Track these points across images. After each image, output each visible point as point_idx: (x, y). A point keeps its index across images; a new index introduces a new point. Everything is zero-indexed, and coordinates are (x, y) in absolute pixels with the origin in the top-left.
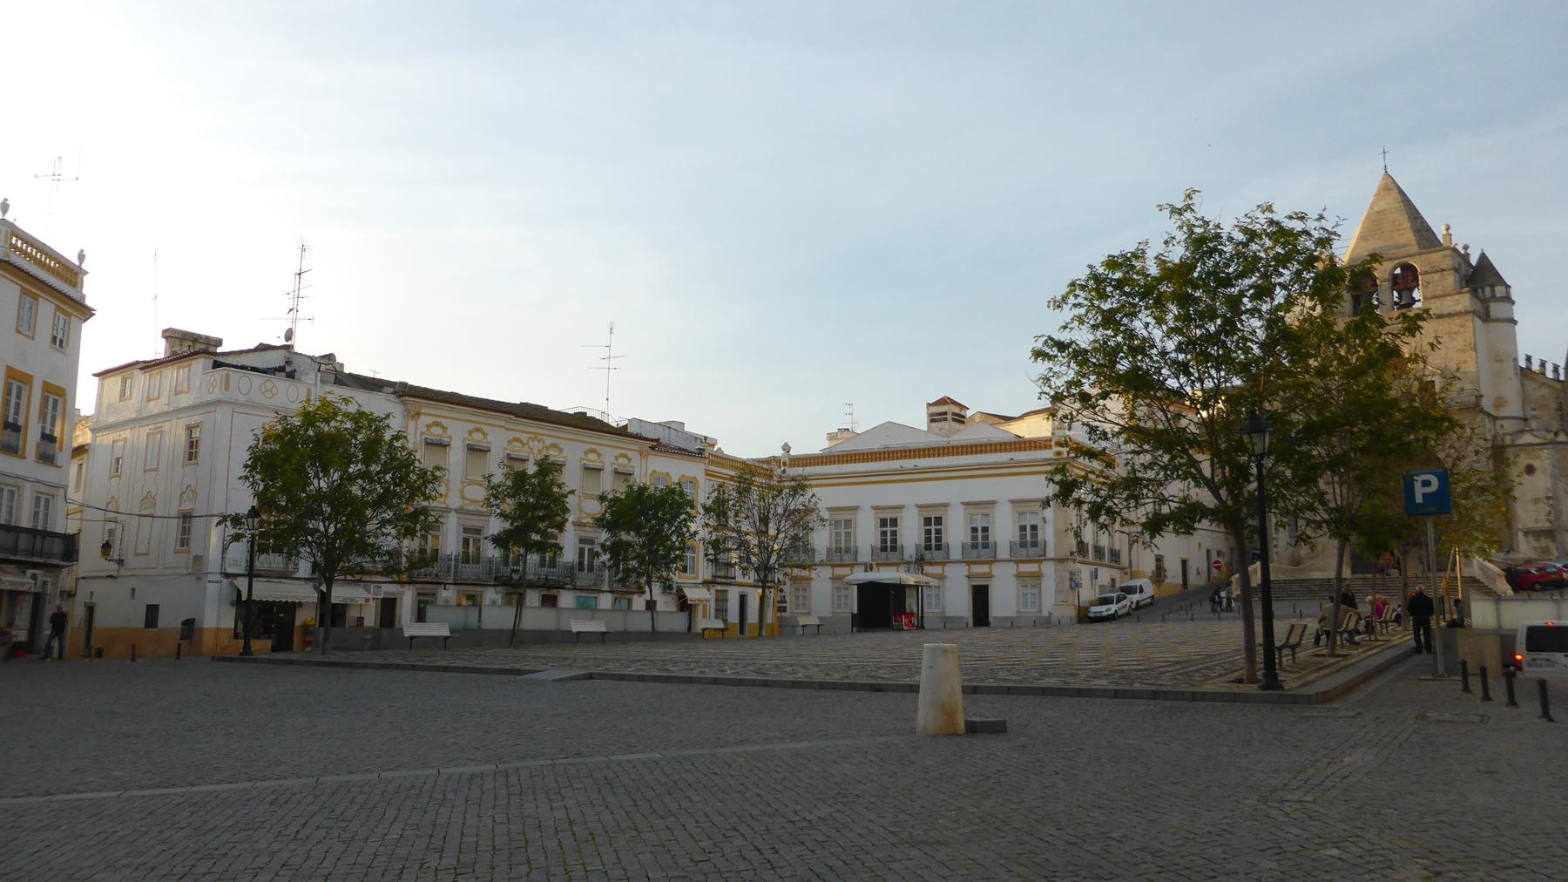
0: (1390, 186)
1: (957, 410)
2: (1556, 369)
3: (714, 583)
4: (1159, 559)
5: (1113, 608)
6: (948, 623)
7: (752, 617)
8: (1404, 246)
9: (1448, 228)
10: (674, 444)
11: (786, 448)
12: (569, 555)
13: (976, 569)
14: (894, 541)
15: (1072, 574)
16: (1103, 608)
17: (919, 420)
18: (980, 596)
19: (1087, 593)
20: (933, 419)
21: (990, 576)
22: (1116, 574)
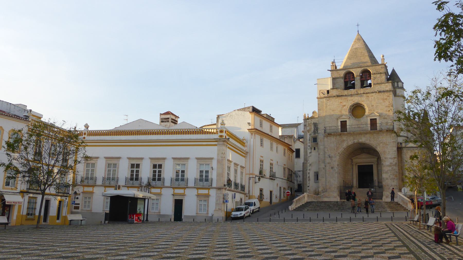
0: (360, 39)
1: (174, 118)
3: (27, 192)
4: (261, 190)
5: (243, 213)
6: (161, 221)
7: (53, 211)
8: (365, 63)
9: (383, 56)
10: (12, 113)
11: (87, 126)
14: (137, 175)
15: (224, 195)
16: (238, 213)
17: (156, 120)
18: (178, 204)
19: (231, 205)
20: (162, 121)
21: (184, 195)
22: (243, 196)
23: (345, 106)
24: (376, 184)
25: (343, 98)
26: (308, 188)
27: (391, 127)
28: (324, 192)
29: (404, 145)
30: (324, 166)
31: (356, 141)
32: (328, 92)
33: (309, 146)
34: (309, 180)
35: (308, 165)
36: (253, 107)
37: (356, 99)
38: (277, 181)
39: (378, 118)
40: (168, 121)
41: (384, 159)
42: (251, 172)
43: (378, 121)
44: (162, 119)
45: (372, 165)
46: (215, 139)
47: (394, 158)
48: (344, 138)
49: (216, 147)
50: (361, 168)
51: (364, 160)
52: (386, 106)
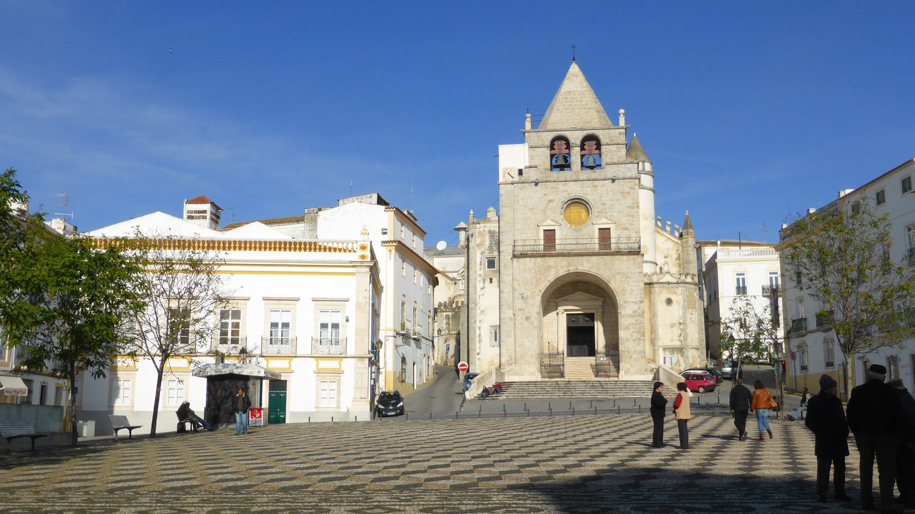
12: (97, 367)
23: (551, 201)
26: (478, 357)
27: (636, 246)
28: (511, 364)
29: (655, 279)
31: (572, 269)
32: (520, 172)
33: (480, 275)
34: (480, 341)
35: (478, 312)
37: (575, 190)
40: (205, 218)
41: (622, 303)
43: (613, 234)
48: (551, 261)
49: (353, 278)
52: (628, 207)
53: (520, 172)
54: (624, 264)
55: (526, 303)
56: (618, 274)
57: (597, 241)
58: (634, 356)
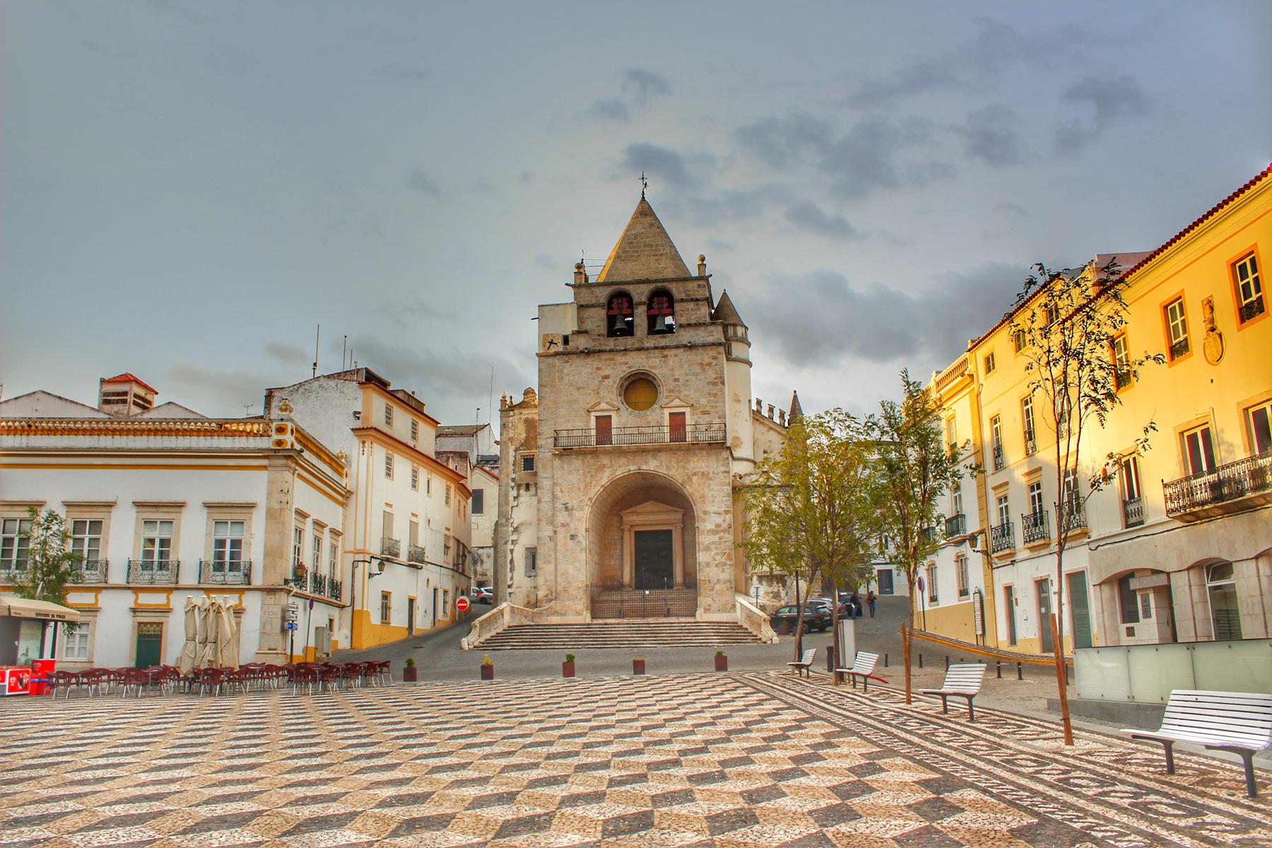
1: (142, 392)
2: (782, 415)
4: (386, 596)
13: (147, 599)
17: (91, 397)
23: (607, 377)
24: (678, 578)
25: (604, 356)
26: (510, 590)
27: (720, 435)
30: (551, 534)
32: (566, 340)
33: (513, 480)
34: (512, 570)
36: (368, 371)
38: (428, 572)
39: (687, 410)
40: (124, 402)
41: (701, 514)
42: (359, 546)
43: (689, 420)
44: (106, 394)
45: (670, 531)
46: (261, 450)
47: (726, 512)
49: (264, 474)
50: (642, 537)
51: (650, 517)
53: (566, 340)
54: (699, 463)
55: (571, 515)
56: (695, 474)
57: (667, 430)
58: (717, 587)
